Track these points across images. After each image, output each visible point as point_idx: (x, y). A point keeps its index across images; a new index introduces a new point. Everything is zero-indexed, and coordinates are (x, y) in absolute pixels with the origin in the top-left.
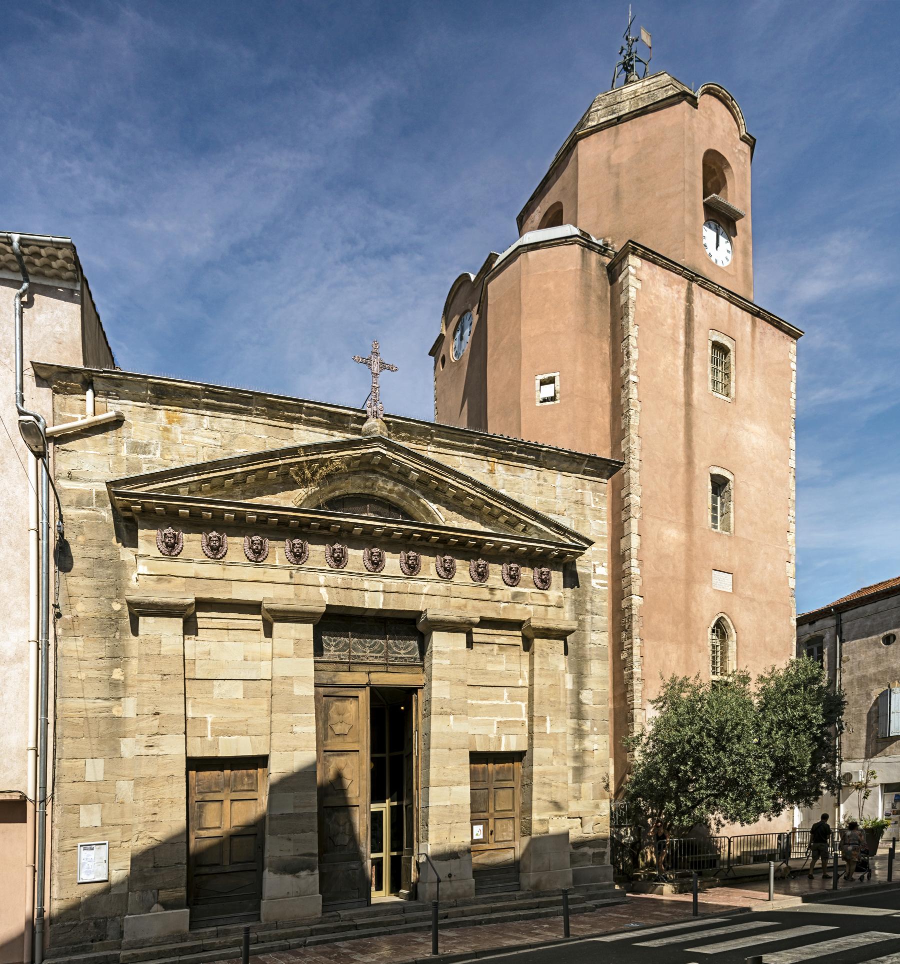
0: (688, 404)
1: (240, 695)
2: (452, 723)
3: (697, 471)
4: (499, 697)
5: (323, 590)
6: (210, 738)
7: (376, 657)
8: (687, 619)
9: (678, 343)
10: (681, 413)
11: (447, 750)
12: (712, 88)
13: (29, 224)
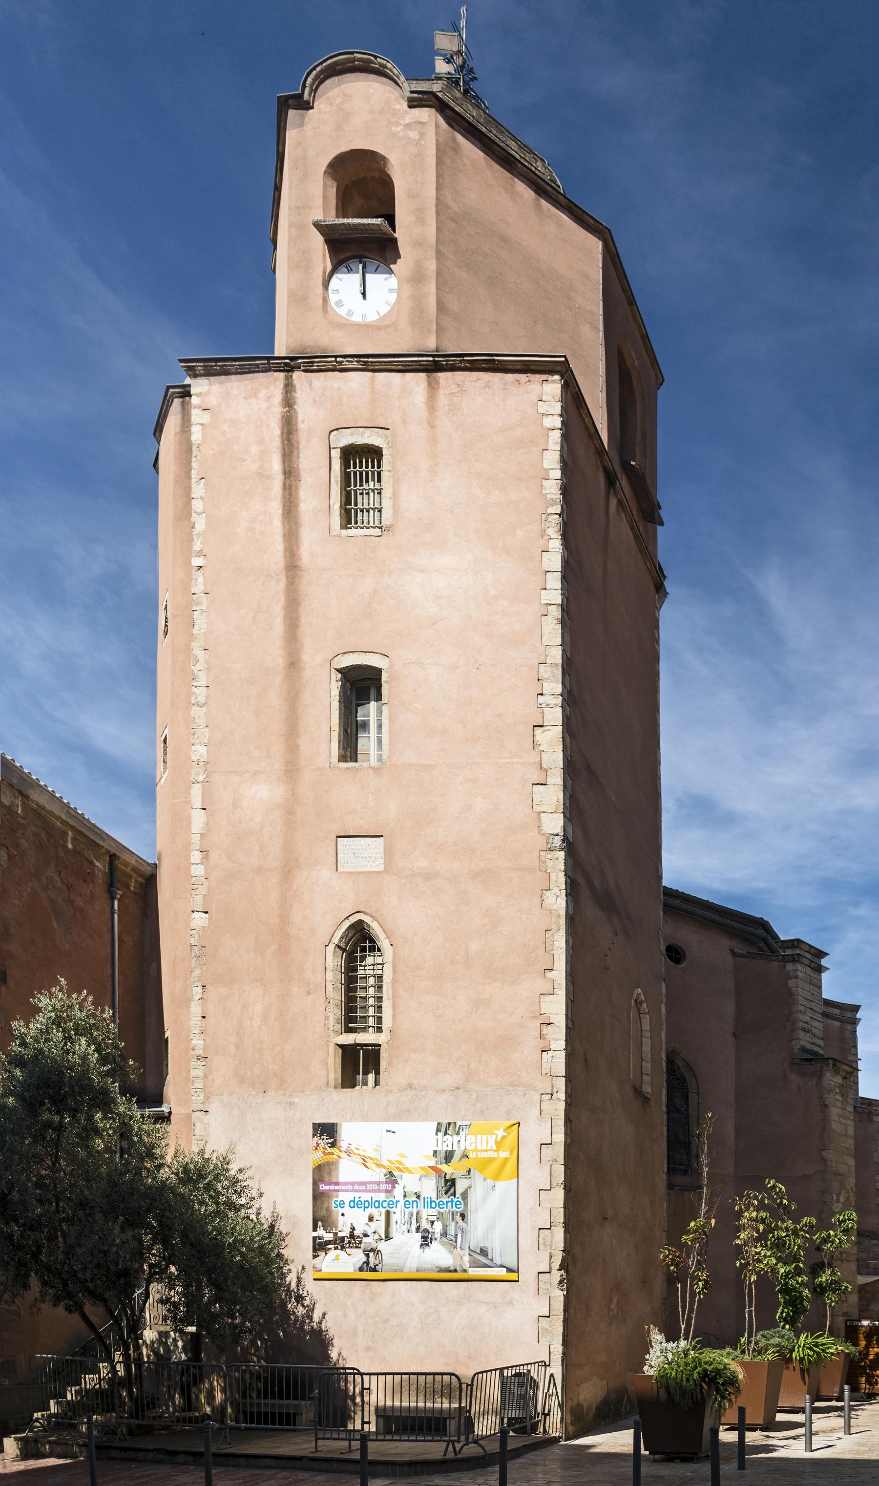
0: (293, 567)
3: (307, 673)
8: (283, 937)
9: (269, 477)
12: (336, 64)
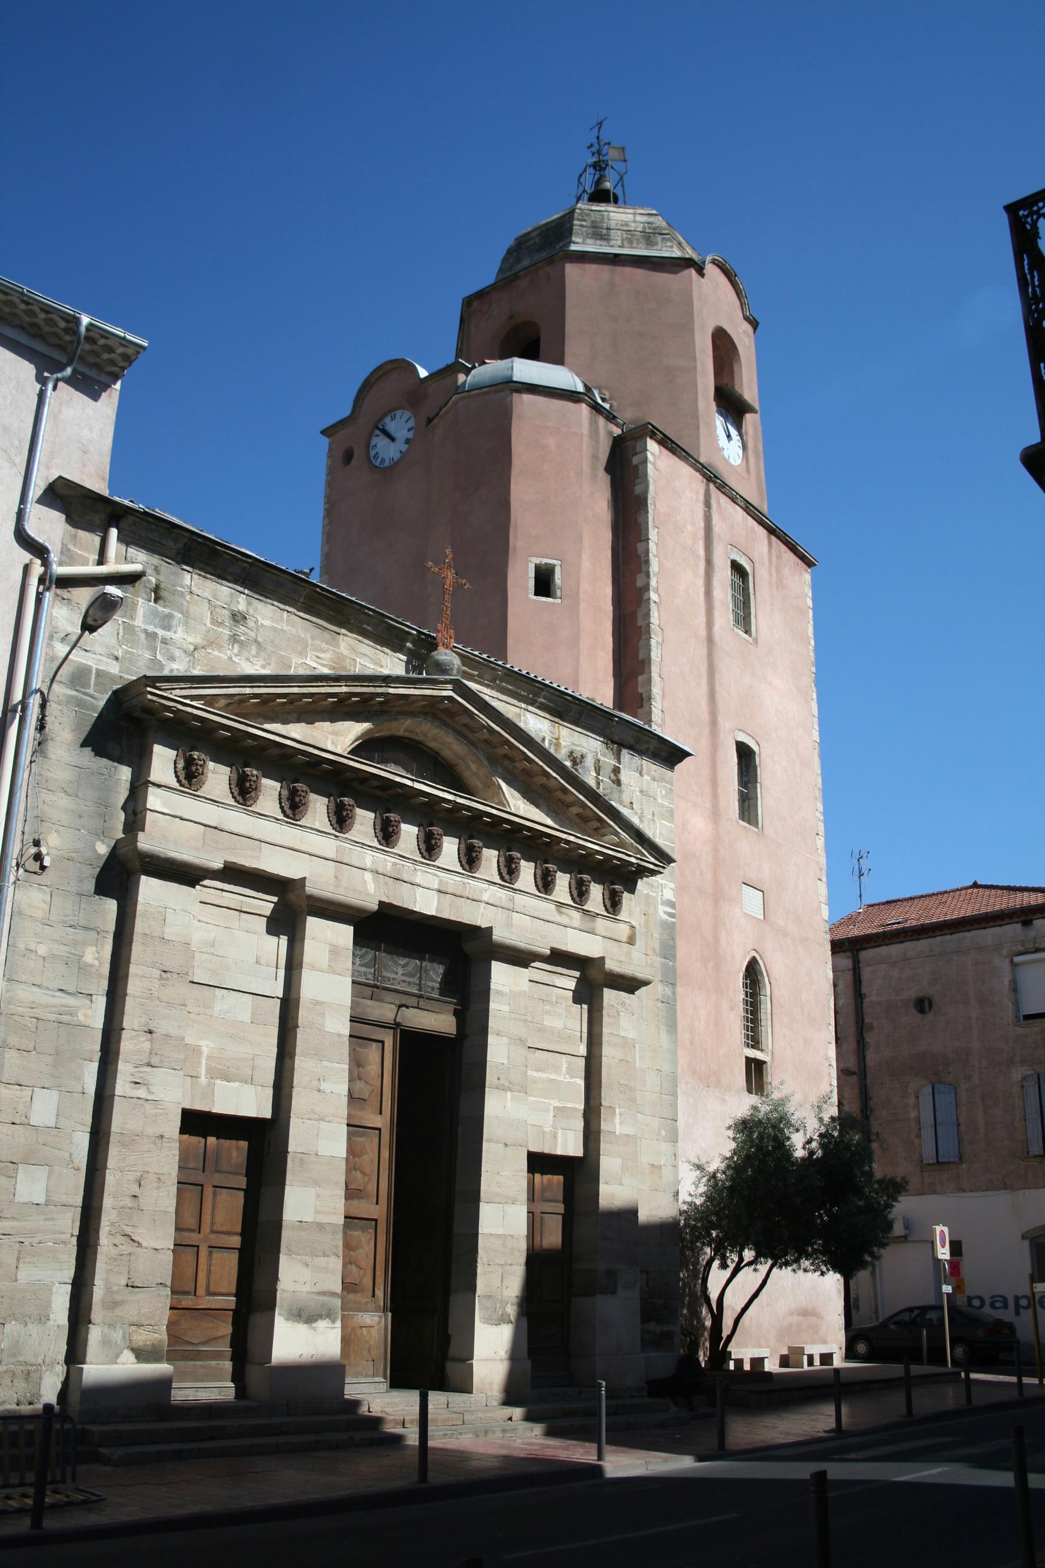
0: (710, 640)
1: (246, 1017)
2: (509, 1104)
4: (557, 1069)
5: (368, 876)
6: (203, 1080)
7: (409, 983)
8: (714, 955)
9: (697, 557)
10: (703, 651)
11: (502, 1146)
13: (1038, 1025)
